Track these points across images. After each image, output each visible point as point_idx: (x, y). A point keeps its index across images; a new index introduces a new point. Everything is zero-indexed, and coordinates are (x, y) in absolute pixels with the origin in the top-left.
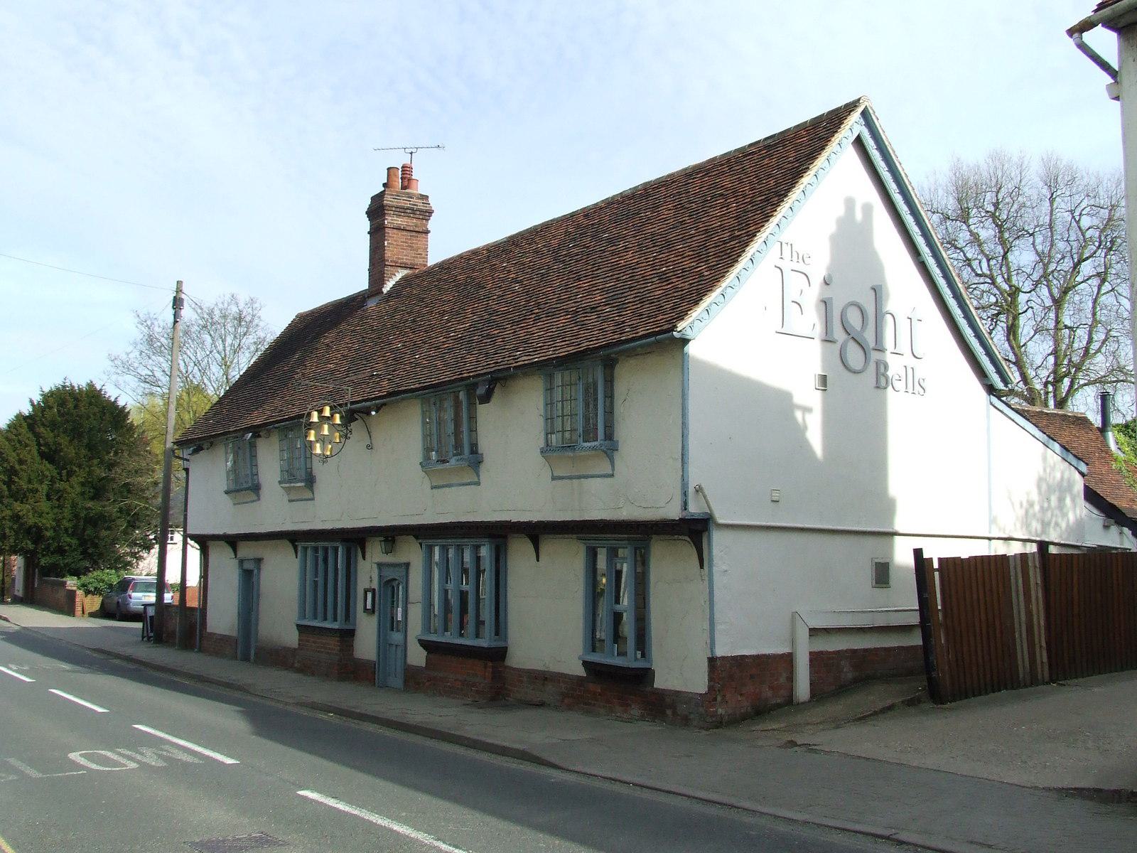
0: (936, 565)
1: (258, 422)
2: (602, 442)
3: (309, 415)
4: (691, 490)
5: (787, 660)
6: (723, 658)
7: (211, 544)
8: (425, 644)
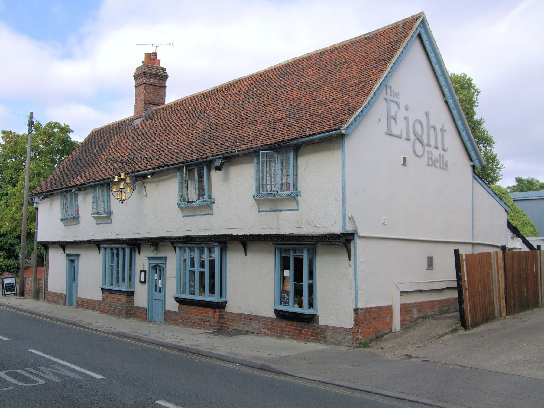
0: (464, 258)
1: (80, 182)
2: (292, 191)
3: (114, 178)
4: (347, 218)
5: (389, 309)
6: (362, 309)
8: (178, 300)
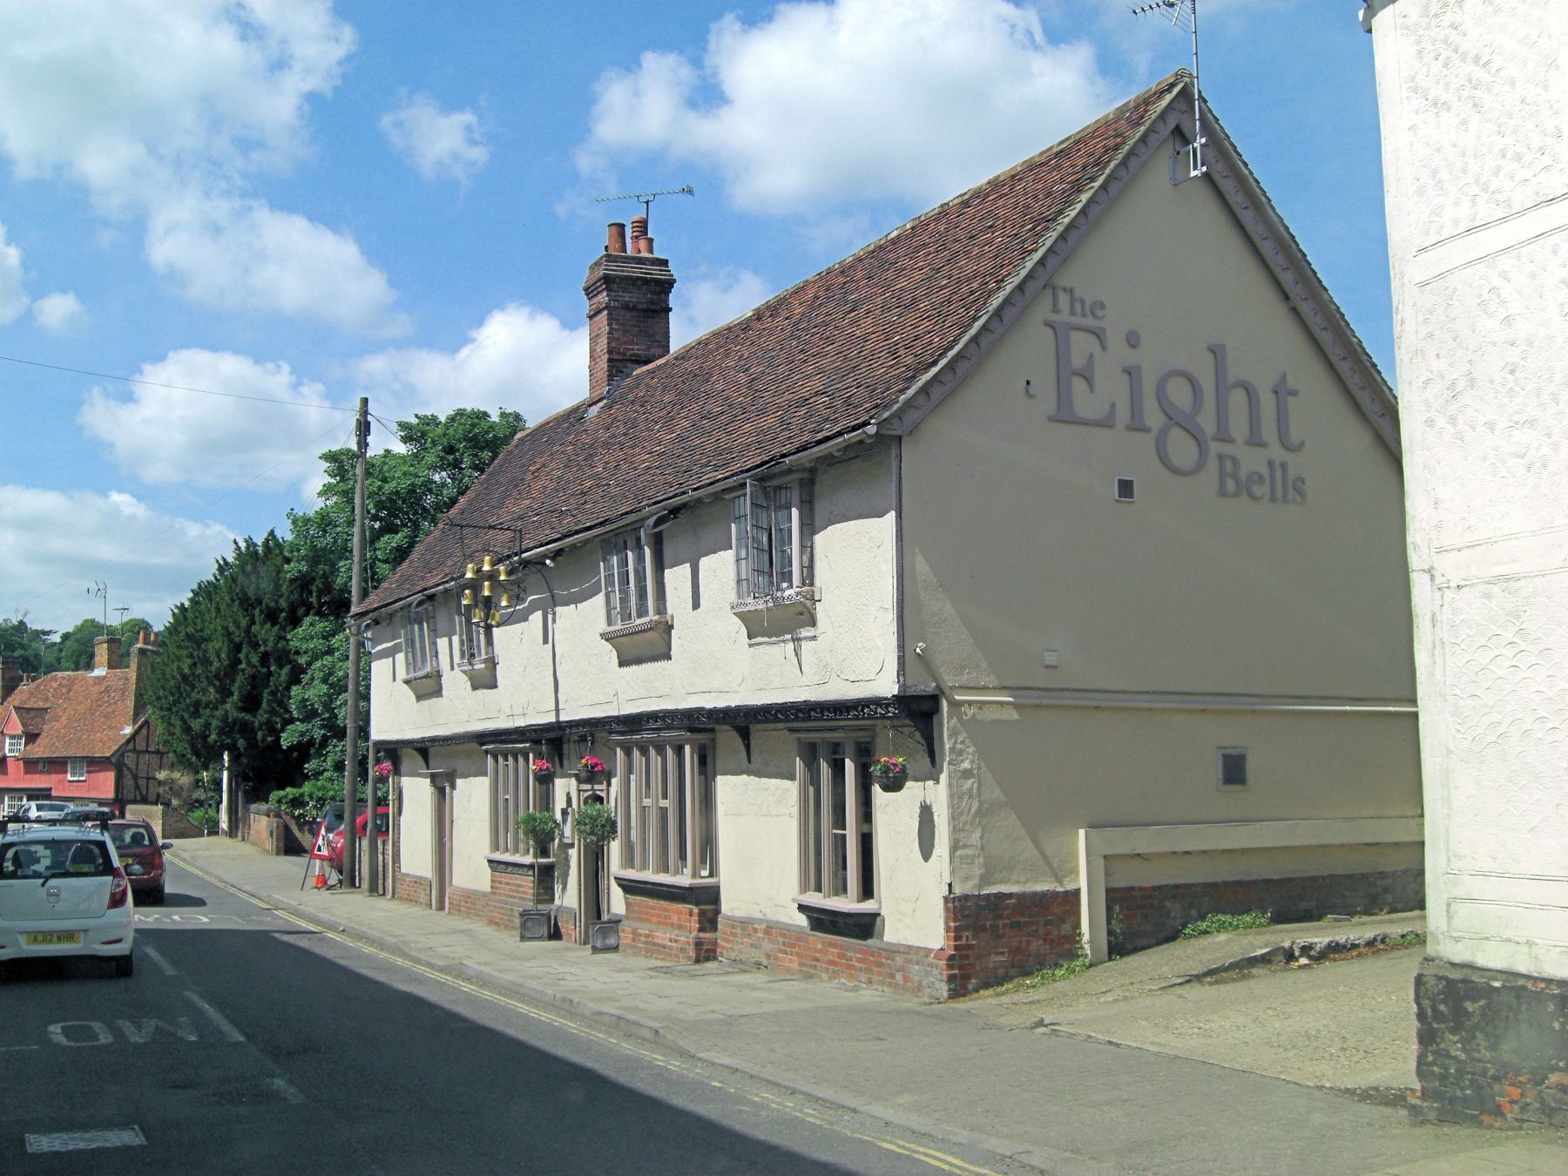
7: (757, 731)
